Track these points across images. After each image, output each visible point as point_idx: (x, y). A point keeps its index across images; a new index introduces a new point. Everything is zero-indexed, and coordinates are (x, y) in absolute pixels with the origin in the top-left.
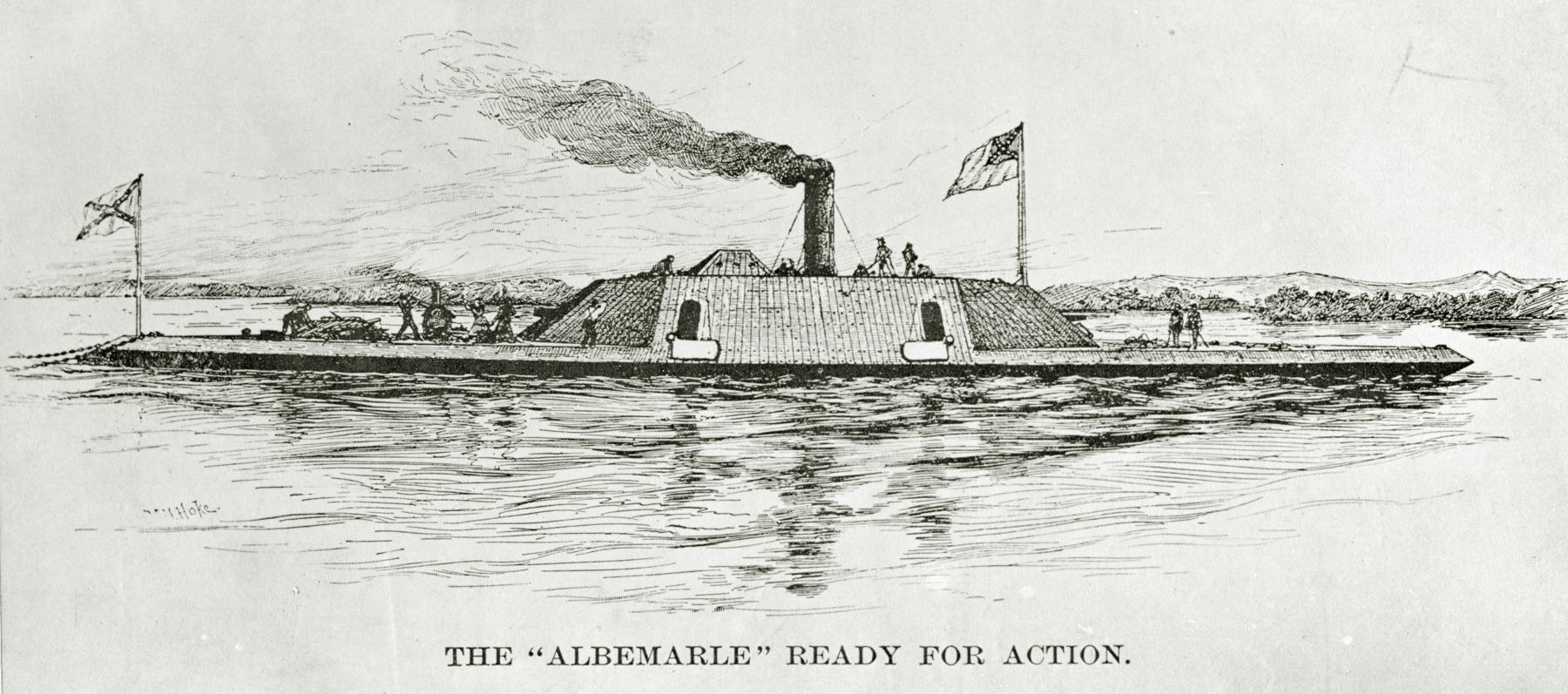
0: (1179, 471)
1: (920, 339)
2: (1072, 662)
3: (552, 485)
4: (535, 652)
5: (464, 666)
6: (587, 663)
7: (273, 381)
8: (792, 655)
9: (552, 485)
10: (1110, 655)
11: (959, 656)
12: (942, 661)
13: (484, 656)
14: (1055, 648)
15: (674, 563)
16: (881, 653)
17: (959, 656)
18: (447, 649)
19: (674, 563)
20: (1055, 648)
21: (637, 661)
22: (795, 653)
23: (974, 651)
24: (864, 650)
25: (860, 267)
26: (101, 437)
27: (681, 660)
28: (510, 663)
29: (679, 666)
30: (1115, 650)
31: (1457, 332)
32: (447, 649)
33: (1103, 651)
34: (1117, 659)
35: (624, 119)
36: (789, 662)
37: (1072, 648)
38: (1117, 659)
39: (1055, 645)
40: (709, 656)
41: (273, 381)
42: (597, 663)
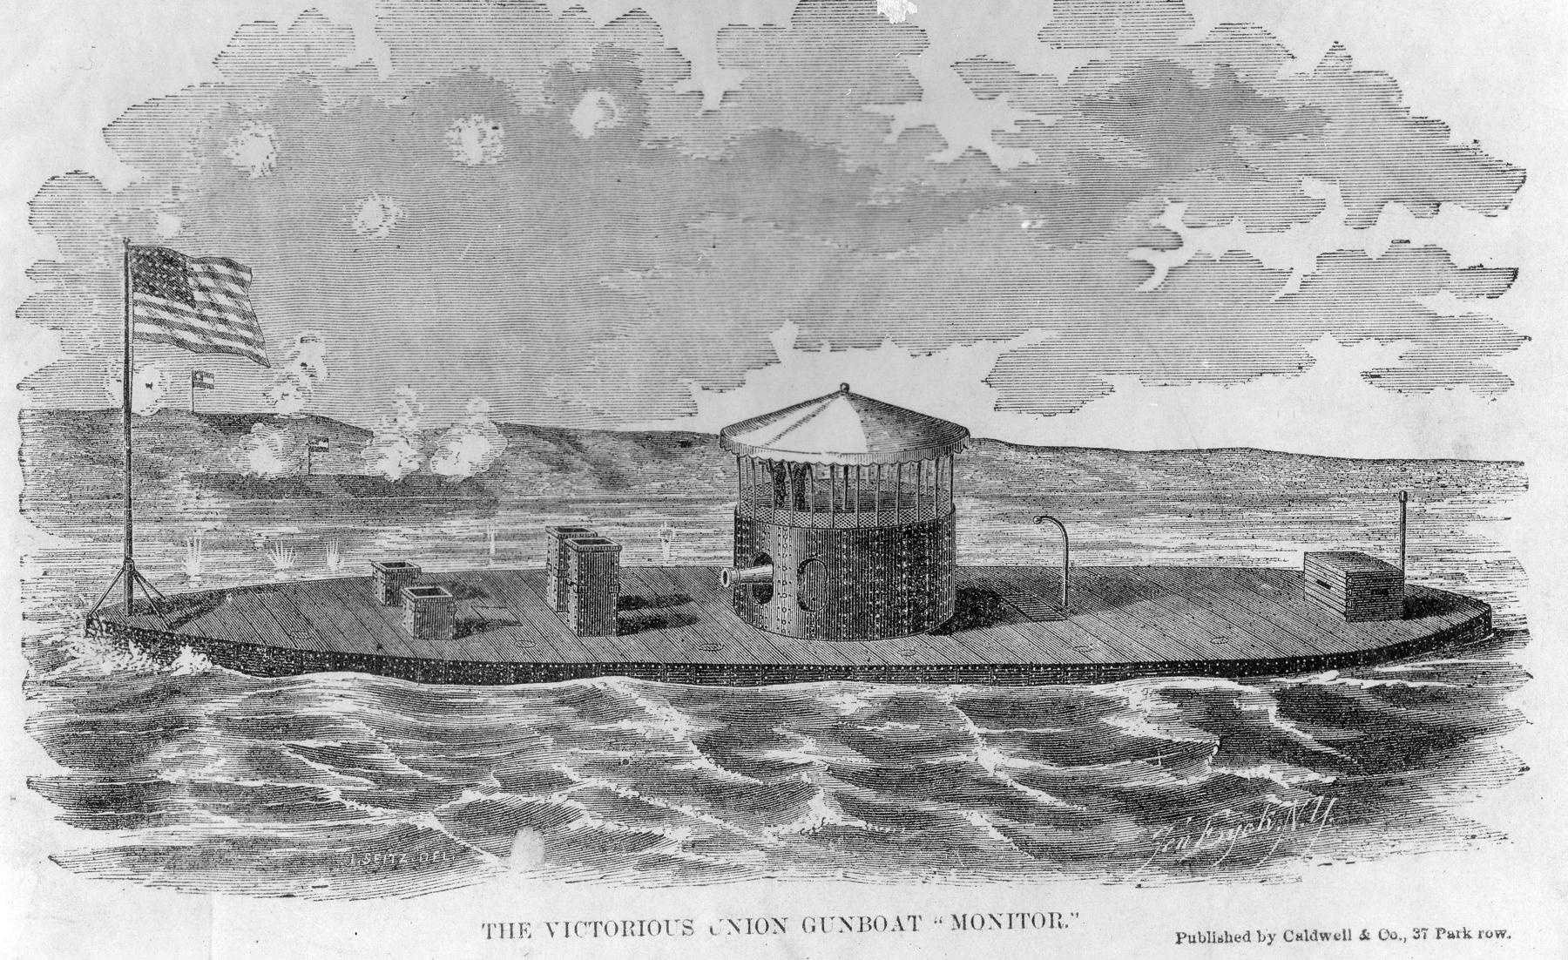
1: (813, 467)
2: (667, 921)
7: (903, 803)
11: (1044, 920)
14: (595, 923)
15: (1501, 934)
16: (988, 921)
17: (1044, 920)
18: (909, 917)
19: (1501, 934)
20: (595, 923)
22: (864, 922)
23: (1056, 917)
26: (814, 416)
29: (548, 921)
30: (782, 922)
31: (88, 831)
32: (909, 917)
33: (772, 923)
37: (641, 922)
41: (903, 803)
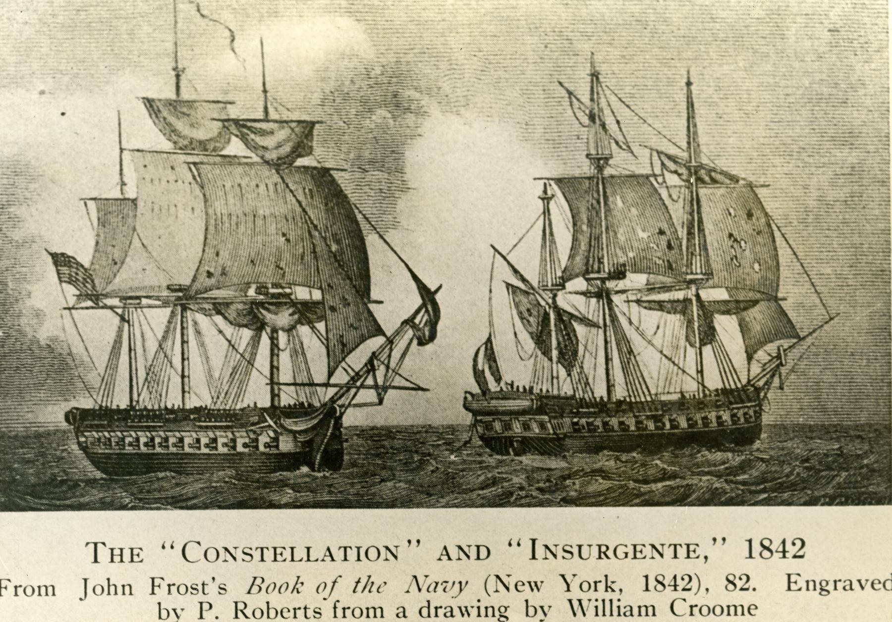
0: (644, 387)
3: (719, 361)
4: (168, 546)
5: (454, 561)
6: (301, 560)
8: (112, 555)
9: (719, 361)
10: (228, 554)
12: (183, 558)
13: (121, 555)
14: (96, 544)
17: (615, 551)
21: (649, 556)
24: (481, 548)
25: (30, 297)
27: (451, 557)
28: (141, 561)
29: (333, 562)
30: (394, 550)
34: (235, 559)
35: (277, 214)
36: (343, 559)
38: (662, 555)
39: (675, 543)
40: (287, 554)
42: (635, 557)
